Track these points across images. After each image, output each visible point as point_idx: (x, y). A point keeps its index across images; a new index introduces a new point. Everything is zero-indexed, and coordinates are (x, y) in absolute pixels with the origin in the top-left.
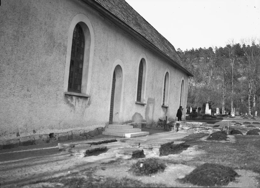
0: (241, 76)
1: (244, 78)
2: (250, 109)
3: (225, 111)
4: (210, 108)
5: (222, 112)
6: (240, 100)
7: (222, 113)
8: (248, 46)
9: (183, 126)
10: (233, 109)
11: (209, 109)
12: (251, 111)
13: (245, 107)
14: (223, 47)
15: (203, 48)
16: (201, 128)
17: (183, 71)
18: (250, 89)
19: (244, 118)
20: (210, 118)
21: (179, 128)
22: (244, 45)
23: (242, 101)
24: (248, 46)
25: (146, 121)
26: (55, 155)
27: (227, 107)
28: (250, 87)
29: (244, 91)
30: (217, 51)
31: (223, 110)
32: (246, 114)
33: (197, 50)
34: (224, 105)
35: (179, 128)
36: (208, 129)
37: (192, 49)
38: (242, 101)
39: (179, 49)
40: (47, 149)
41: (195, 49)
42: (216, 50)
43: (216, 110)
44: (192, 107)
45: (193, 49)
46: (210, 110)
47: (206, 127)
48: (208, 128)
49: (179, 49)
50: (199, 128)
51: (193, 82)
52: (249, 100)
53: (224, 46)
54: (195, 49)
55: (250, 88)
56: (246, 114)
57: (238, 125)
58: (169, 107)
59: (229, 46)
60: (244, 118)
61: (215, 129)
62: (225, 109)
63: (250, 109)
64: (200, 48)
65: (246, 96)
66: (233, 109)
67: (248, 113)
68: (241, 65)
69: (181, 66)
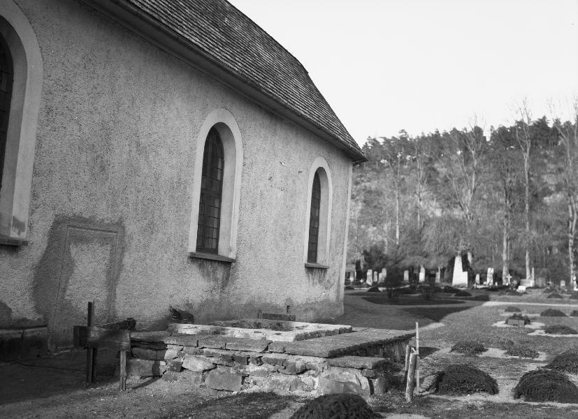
0: (550, 193)
1: (559, 196)
2: (574, 270)
3: (509, 277)
4: (466, 266)
5: (504, 278)
6: (550, 249)
7: (502, 282)
8: (568, 123)
9: (181, 354)
10: (531, 271)
11: (464, 270)
12: (576, 275)
13: (560, 265)
14: (508, 126)
15: (460, 129)
16: (269, 361)
17: (326, 140)
18: (572, 221)
19: (549, 297)
20: (453, 295)
21: (162, 363)
22: (557, 122)
23: (556, 251)
24: (568, 123)
25: (46, 326)
26: (80, 392)
27: (515, 266)
28: (571, 215)
29: (559, 228)
30: (494, 135)
31: (504, 273)
32: (563, 284)
33: (446, 134)
34: (507, 261)
35: (162, 363)
36: (304, 370)
37: (434, 133)
38: (556, 251)
39: (403, 131)
40: (425, 309)
41: (441, 132)
42: (492, 134)
43: (486, 273)
44: (424, 266)
45: (438, 132)
46: (466, 273)
47: (291, 359)
48: (299, 364)
49: (403, 131)
50: (259, 361)
51: (436, 208)
52: (570, 249)
53: (510, 124)
54: (441, 132)
55: (573, 217)
56: (563, 284)
57: (516, 322)
58: (242, 260)
59: (521, 123)
60: (549, 297)
61: (335, 371)
62: (510, 272)
63: (574, 270)
64: (455, 129)
65: (564, 241)
66: (531, 271)
67: (568, 280)
68: (552, 166)
69: (294, 112)
